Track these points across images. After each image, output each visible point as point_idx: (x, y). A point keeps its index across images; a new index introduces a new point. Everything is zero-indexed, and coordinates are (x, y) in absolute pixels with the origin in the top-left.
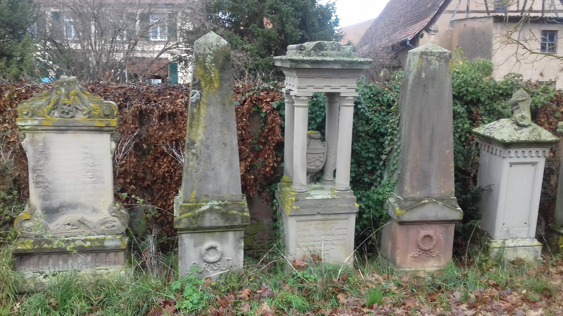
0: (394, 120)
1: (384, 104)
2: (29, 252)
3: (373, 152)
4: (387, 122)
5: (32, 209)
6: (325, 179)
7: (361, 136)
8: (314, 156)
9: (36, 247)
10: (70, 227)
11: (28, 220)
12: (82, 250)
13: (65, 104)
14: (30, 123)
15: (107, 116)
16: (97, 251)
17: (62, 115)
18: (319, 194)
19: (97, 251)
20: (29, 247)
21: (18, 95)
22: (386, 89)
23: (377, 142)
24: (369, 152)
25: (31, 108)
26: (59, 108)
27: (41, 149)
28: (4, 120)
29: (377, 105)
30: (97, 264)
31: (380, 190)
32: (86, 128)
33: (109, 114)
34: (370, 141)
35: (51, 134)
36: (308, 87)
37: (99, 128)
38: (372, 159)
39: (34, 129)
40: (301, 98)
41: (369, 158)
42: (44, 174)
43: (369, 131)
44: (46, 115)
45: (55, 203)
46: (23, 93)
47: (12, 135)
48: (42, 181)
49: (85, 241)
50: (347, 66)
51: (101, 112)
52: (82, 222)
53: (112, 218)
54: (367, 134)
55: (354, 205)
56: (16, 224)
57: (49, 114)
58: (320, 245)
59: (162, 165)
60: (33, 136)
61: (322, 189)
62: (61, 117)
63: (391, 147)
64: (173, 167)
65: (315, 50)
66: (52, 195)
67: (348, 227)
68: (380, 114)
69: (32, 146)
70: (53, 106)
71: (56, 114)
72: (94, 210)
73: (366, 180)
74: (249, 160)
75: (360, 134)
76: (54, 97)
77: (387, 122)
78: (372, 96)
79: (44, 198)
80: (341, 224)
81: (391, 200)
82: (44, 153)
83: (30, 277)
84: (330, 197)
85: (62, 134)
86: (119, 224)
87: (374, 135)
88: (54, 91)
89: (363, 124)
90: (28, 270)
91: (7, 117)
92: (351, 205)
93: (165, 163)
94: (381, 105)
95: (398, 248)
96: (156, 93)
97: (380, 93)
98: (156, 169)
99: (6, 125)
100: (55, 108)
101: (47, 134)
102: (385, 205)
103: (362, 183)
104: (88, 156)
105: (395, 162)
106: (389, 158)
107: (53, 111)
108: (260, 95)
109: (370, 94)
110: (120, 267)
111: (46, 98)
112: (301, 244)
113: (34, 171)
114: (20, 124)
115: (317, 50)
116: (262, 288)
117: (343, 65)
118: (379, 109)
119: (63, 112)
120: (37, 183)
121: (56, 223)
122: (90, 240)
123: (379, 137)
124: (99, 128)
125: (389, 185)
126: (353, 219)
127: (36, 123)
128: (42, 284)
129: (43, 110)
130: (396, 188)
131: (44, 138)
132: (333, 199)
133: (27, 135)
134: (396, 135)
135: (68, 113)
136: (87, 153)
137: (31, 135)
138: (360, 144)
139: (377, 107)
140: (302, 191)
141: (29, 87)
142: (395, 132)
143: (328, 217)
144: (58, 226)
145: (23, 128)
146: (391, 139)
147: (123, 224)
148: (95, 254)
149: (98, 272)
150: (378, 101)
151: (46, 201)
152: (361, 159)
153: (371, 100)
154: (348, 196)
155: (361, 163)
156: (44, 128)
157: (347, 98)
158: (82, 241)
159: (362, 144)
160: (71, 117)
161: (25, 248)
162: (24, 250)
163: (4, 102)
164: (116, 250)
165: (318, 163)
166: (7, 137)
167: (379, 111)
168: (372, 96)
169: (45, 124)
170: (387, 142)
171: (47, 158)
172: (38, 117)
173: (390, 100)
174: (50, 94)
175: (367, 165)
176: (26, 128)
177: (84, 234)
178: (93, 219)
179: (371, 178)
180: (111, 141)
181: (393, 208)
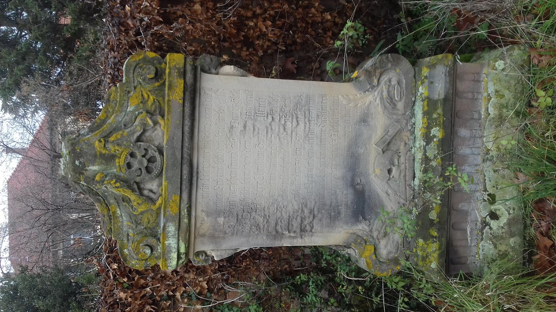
2: (444, 247)
5: (355, 242)
9: (435, 234)
10: (394, 170)
11: (375, 249)
12: (448, 146)
13: (129, 166)
14: (172, 242)
15: (159, 75)
16: (451, 113)
17: (156, 172)
19: (451, 113)
20: (433, 248)
21: (123, 275)
25: (138, 238)
26: (138, 179)
27: (233, 222)
28: (169, 298)
30: (476, 116)
32: (187, 122)
33: (153, 69)
35: (200, 199)
37: (187, 94)
39: (187, 233)
42: (285, 216)
44: (154, 208)
45: (345, 196)
46: (119, 267)
47: (196, 285)
48: (299, 218)
49: (428, 138)
51: (149, 87)
52: (387, 146)
53: (383, 86)
56: (383, 271)
57: (153, 201)
59: (261, 30)
60: (203, 236)
62: (160, 175)
64: (265, 11)
66: (328, 202)
69: (224, 238)
70: (133, 191)
71: (153, 185)
72: (364, 120)
76: (112, 189)
79: (333, 217)
82: (240, 214)
83: (492, 247)
85: (200, 174)
86: (396, 75)
88: (96, 187)
90: (475, 250)
91: (164, 293)
93: (256, 25)
96: (120, 31)
98: (267, 43)
99: (178, 295)
100: (139, 190)
101: (199, 208)
104: (250, 124)
107: (146, 192)
110: (485, 70)
111: (113, 206)
113: (278, 235)
114: (174, 263)
119: (148, 170)
120: (303, 230)
121: (383, 195)
122: (428, 128)
124: (187, 94)
127: (172, 229)
128: (510, 223)
129: (142, 213)
131: (208, 214)
133: (199, 248)
135: (151, 160)
136: (245, 127)
137: (198, 240)
141: (108, 257)
144: (390, 191)
145: (183, 256)
147: (396, 63)
148: (457, 119)
149: (492, 116)
151: (339, 213)
156: (185, 212)
158: (428, 143)
160: (161, 152)
161: (436, 255)
162: (440, 256)
163: (136, 299)
164: (453, 76)
166: (200, 293)
169: (176, 210)
171: (250, 209)
172: (158, 224)
174: (105, 198)
176: (183, 250)
177: (411, 143)
178: (380, 123)
180: (217, 74)
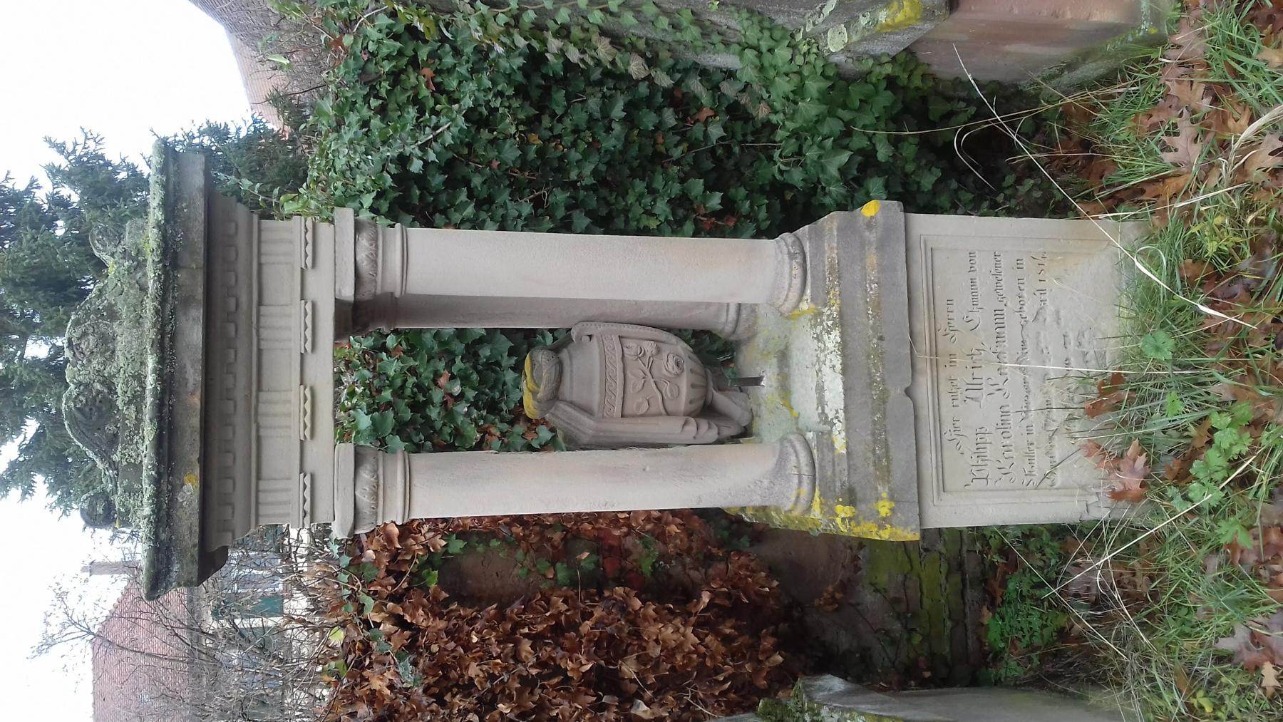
0: (474, 23)
1: (410, 53)
3: (607, 102)
4: (483, 53)
6: (729, 328)
7: (541, 152)
8: (634, 382)
18: (813, 381)
22: (348, 40)
23: (562, 82)
24: (606, 115)
29: (413, 80)
31: (784, 86)
34: (559, 112)
36: (309, 467)
38: (631, 107)
40: (365, 500)
41: (630, 120)
43: (522, 116)
50: (191, 279)
54: (532, 124)
55: (870, 224)
58: (1045, 376)
61: (784, 357)
63: (595, 37)
65: (113, 440)
67: (962, 242)
68: (450, 71)
73: (716, 131)
74: (637, 603)
75: (532, 155)
77: (483, 53)
78: (374, 103)
80: (952, 281)
81: (836, 42)
84: (836, 335)
87: (536, 94)
89: (493, 142)
92: (872, 236)
94: (414, 63)
95: (1055, 15)
97: (363, 69)
102: (851, 67)
103: (728, 149)
105: (664, 22)
106: (641, 45)
108: (376, 562)
109: (366, 113)
112: (1041, 464)
115: (110, 428)
116: (1250, 656)
117: (187, 302)
118: (428, 72)
123: (545, 77)
125: (764, 46)
126: (937, 229)
130: (781, 20)
132: (842, 322)
134: (541, 12)
138: (575, 155)
139: (419, 81)
140: (806, 469)
142: (530, 16)
143: (925, 345)
146: (557, 35)
150: (396, 77)
152: (634, 150)
153: (392, 106)
154: (831, 250)
155: (649, 151)
157: (365, 265)
159: (574, 145)
165: (666, 365)
167: (438, 72)
168: (374, 103)
170: (574, 55)
173: (389, 27)
175: (658, 127)
179: (707, 112)
181: (876, 33)
